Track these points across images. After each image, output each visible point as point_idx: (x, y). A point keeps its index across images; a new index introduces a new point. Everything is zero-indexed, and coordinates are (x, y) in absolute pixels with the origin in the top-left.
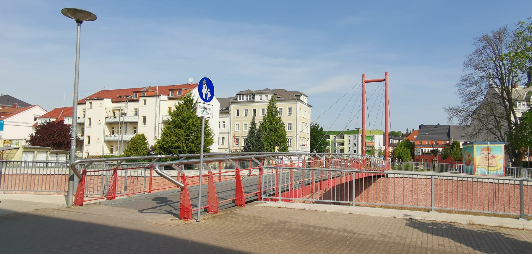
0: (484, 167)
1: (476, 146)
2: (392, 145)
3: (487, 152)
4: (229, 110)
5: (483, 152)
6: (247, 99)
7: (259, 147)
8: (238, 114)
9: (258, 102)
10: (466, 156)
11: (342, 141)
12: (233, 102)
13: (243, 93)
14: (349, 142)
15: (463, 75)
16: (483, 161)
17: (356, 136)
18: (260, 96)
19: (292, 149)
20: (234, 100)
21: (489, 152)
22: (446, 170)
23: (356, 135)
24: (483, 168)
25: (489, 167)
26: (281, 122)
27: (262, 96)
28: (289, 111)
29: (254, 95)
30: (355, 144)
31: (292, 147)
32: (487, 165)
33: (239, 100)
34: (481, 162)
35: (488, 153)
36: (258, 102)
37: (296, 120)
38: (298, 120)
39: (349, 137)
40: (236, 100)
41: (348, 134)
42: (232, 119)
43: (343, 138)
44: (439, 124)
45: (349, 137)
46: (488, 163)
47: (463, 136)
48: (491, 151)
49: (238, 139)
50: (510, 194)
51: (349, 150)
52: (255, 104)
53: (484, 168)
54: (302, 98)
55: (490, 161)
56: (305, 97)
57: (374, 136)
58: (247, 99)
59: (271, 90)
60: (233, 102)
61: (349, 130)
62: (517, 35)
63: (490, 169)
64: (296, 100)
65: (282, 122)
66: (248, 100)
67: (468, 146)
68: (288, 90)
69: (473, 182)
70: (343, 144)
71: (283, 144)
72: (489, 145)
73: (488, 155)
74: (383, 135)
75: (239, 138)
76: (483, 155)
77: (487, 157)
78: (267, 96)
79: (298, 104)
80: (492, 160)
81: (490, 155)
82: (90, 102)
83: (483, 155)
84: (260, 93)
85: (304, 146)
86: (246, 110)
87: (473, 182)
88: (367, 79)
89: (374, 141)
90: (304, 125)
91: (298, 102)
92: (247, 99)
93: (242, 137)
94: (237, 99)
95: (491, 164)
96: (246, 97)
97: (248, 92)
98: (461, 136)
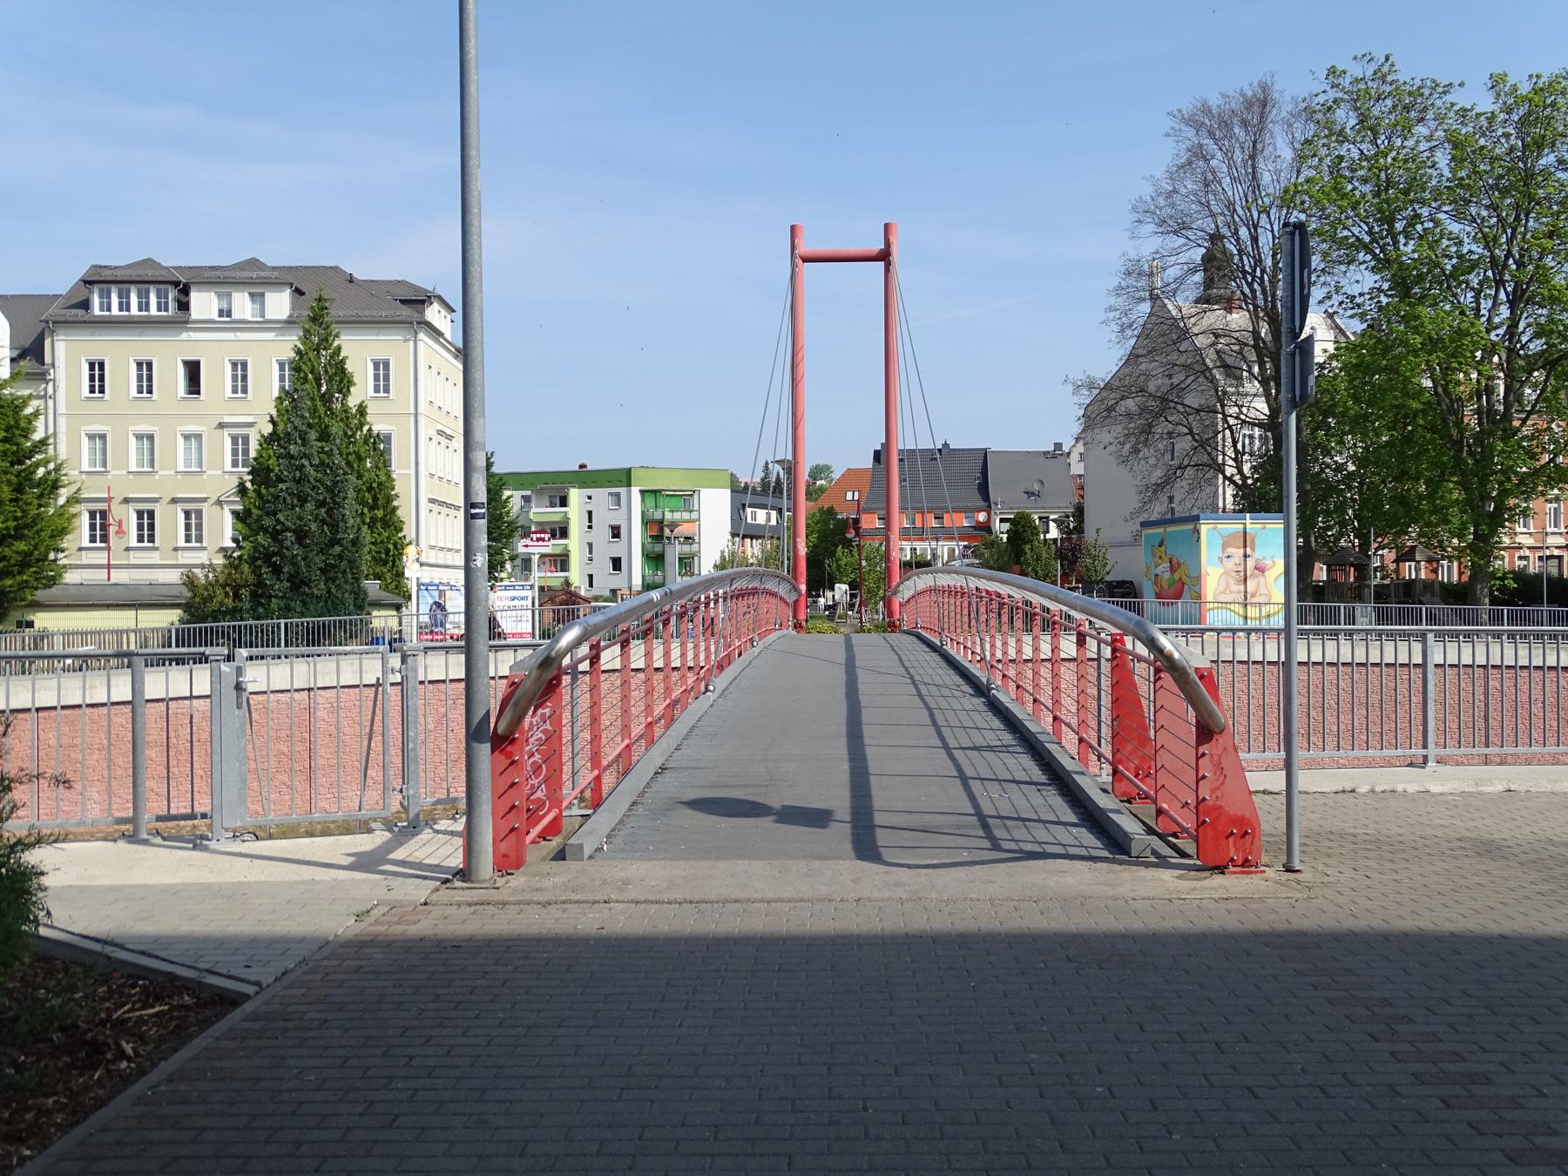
0: (1228, 606)
1: (1208, 530)
2: (753, 534)
3: (1242, 551)
4: (40, 359)
5: (1231, 550)
6: (145, 306)
7: (337, 549)
8: (97, 383)
9: (206, 325)
10: (1159, 570)
11: (557, 518)
12: (66, 322)
13: (107, 275)
14: (590, 521)
15: (1133, 255)
16: (1228, 585)
17: (618, 495)
18: (219, 296)
19: (161, 559)
20: (70, 307)
21: (1249, 551)
22: (217, 639)
23: (622, 490)
24: (1226, 608)
25: (1246, 605)
26: (366, 428)
27: (229, 295)
28: (377, 378)
29: (185, 291)
30: (616, 532)
31: (156, 549)
32: (1240, 598)
33: (97, 311)
34: (1223, 590)
35: (1245, 556)
36: (206, 325)
37: (412, 418)
38: (421, 419)
39: (590, 498)
40: (81, 312)
41: (583, 485)
42: (62, 409)
43: (564, 502)
44: (946, 445)
45: (590, 498)
46: (1246, 592)
47: (1033, 494)
48: (1253, 549)
49: (151, 514)
50: (1326, 701)
51: (591, 559)
52: (194, 335)
53: (1230, 609)
54: (434, 314)
55: (1251, 585)
56: (443, 312)
57: (696, 496)
58: (145, 306)
59: (167, 268)
60: (66, 322)
61: (584, 466)
62: (1317, 114)
63: (1249, 615)
64: (411, 323)
65: (370, 430)
66: (153, 311)
67: (1168, 529)
68: (358, 275)
69: (1341, 667)
70: (562, 531)
71: (386, 534)
72: (1248, 526)
73: (1245, 561)
74: (728, 492)
75: (205, 507)
76: (1230, 564)
77: (1241, 568)
78: (257, 297)
79: (421, 345)
80: (1256, 580)
81: (1250, 563)
82: (251, 291)
83: (1230, 564)
84: (222, 279)
85: (541, 543)
86: (146, 367)
87: (1341, 667)
88: (806, 246)
89: (694, 515)
90: (444, 441)
91: (422, 336)
92: (128, 309)
93: (174, 501)
94: (85, 305)
95: (1252, 596)
96: (120, 297)
97: (150, 274)
98: (1027, 493)
